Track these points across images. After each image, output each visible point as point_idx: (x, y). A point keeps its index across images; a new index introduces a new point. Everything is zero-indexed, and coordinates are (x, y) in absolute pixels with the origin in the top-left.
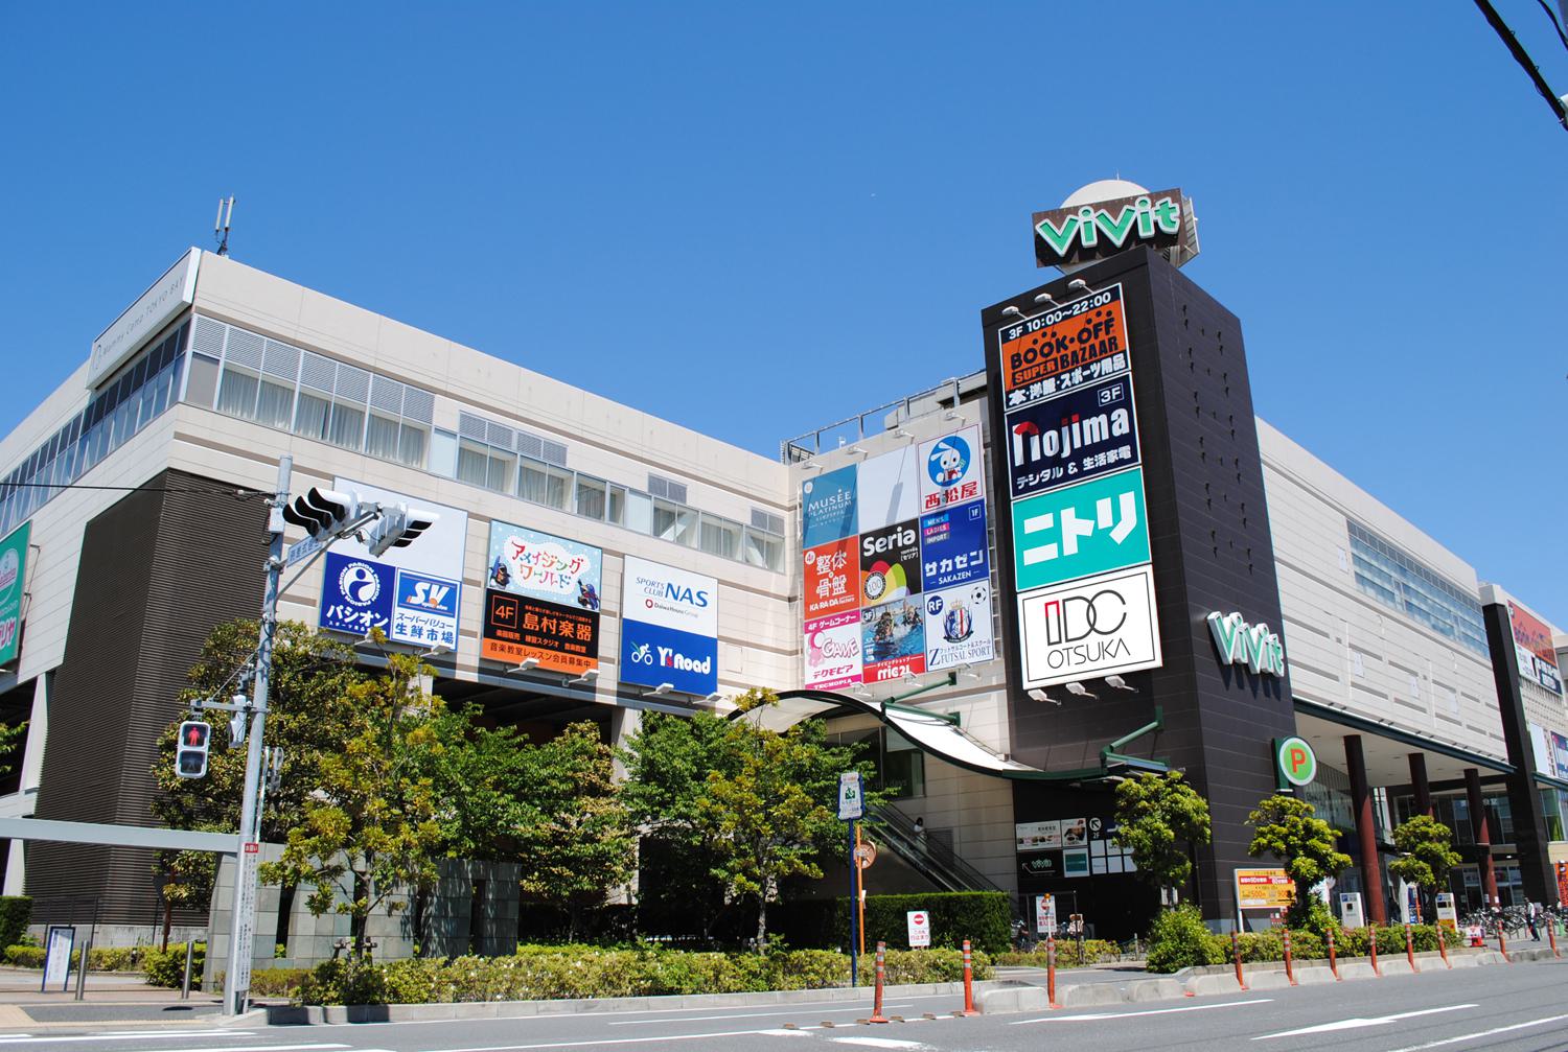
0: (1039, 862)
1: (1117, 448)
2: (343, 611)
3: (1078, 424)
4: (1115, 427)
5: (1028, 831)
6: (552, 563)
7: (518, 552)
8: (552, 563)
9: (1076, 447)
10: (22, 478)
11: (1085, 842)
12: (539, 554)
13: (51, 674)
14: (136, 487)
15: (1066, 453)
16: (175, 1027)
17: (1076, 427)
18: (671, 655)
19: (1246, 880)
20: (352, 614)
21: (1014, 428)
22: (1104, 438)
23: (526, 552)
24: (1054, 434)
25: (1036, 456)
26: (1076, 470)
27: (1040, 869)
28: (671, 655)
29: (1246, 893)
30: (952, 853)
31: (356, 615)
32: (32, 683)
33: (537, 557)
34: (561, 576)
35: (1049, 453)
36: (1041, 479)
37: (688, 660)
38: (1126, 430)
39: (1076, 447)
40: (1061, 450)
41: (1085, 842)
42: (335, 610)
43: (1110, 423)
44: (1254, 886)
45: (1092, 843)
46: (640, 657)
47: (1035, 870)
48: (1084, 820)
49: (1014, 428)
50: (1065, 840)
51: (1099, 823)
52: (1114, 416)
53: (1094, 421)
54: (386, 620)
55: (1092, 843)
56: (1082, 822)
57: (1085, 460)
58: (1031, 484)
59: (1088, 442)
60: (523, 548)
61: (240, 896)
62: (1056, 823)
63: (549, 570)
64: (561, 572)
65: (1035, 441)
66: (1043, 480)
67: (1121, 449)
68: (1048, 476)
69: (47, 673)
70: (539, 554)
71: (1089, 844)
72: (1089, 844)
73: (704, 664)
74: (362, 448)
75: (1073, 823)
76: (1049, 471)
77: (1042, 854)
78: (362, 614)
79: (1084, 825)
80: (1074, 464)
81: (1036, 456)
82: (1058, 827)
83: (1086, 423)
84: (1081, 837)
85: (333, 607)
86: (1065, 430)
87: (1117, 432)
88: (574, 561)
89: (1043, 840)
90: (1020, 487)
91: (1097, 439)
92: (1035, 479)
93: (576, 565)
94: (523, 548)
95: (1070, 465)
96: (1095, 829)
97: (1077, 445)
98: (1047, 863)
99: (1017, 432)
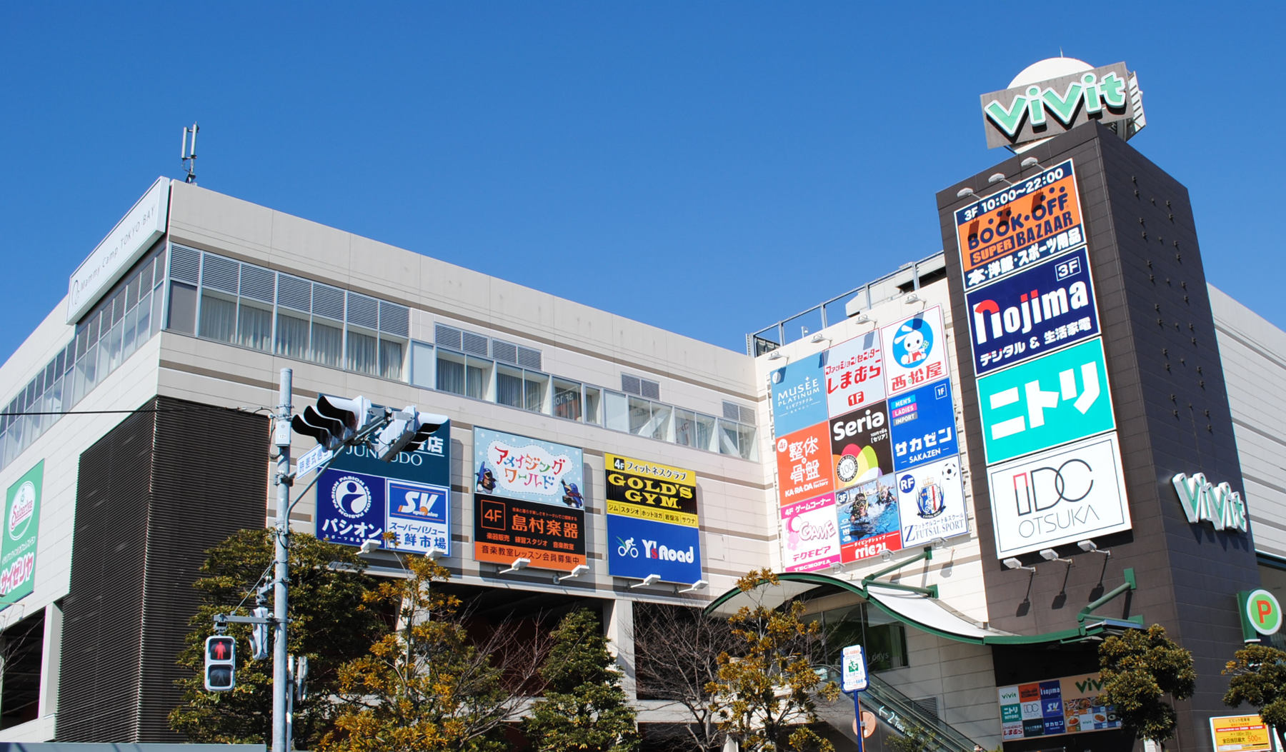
1: (1077, 320)
2: (337, 524)
4: (1074, 299)
6: (535, 465)
7: (502, 457)
8: (535, 465)
12: (522, 458)
13: (59, 603)
15: (1027, 328)
17: (1035, 302)
18: (655, 547)
22: (1055, 315)
23: (509, 456)
24: (1013, 310)
25: (997, 333)
28: (655, 547)
33: (520, 460)
34: (545, 477)
36: (1004, 355)
37: (672, 551)
38: (1085, 302)
40: (1022, 326)
43: (1069, 297)
46: (626, 551)
49: (975, 307)
52: (1072, 289)
53: (1053, 295)
59: (1048, 316)
60: (506, 452)
63: (532, 472)
64: (545, 474)
65: (995, 318)
66: (1006, 356)
67: (1081, 321)
70: (522, 458)
73: (688, 553)
74: (690, 446)
76: (1011, 346)
78: (356, 526)
80: (1035, 338)
81: (997, 333)
83: (1045, 298)
85: (327, 521)
86: (1025, 306)
87: (1076, 305)
88: (556, 463)
93: (558, 466)
94: (506, 452)
98: (1006, 718)
99: (978, 310)
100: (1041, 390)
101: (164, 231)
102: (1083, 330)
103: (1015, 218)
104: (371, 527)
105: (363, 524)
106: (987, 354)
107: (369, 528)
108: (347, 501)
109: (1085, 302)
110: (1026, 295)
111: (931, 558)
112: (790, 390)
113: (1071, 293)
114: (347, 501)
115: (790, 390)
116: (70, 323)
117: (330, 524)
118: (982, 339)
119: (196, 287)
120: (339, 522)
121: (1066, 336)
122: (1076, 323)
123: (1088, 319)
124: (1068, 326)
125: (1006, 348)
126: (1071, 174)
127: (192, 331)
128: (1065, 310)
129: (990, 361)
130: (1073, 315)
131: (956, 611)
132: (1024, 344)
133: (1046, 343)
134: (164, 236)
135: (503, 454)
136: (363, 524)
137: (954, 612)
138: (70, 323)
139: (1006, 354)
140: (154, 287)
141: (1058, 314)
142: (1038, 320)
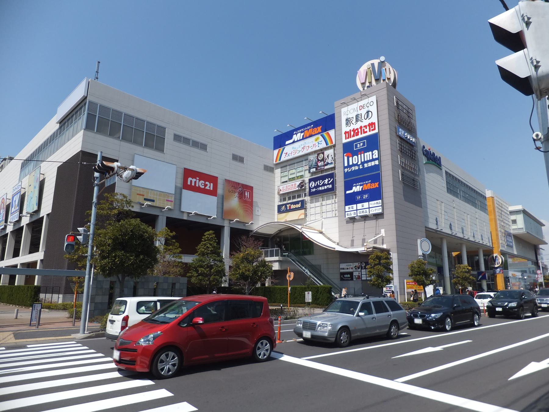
0: (346, 275)
1: (374, 161)
2: (319, 182)
3: (360, 155)
4: (374, 155)
5: (343, 266)
9: (345, 166)
10: (31, 159)
11: (360, 270)
13: (48, 215)
14: (64, 162)
15: (359, 163)
16: (52, 340)
17: (362, 155)
19: (409, 283)
20: (322, 182)
21: (345, 154)
22: (370, 159)
23: (288, 154)
24: (356, 157)
25: (351, 163)
26: (362, 167)
27: (347, 278)
29: (408, 287)
30: (321, 272)
31: (323, 181)
32: (43, 217)
35: (355, 163)
36: (352, 169)
37: (295, 205)
38: (377, 157)
39: (345, 166)
40: (358, 162)
41: (360, 270)
42: (317, 183)
43: (373, 154)
44: (411, 285)
45: (362, 270)
47: (345, 278)
48: (360, 263)
49: (345, 154)
50: (354, 269)
51: (364, 264)
52: (374, 152)
53: (368, 153)
54: (332, 179)
55: (362, 270)
56: (359, 264)
57: (365, 164)
58: (349, 171)
59: (366, 160)
60: (287, 153)
61: (356, 138)
62: (352, 264)
65: (350, 158)
66: (352, 170)
67: (376, 161)
68: (354, 169)
69: (47, 215)
71: (361, 270)
72: (361, 270)
73: (299, 204)
74: (372, 215)
75: (357, 264)
76: (354, 167)
77: (347, 273)
78: (325, 181)
79: (360, 265)
80: (361, 165)
81: (351, 163)
82: (352, 265)
83: (366, 154)
84: (359, 268)
85: (316, 182)
86: (359, 156)
87: (374, 157)
89: (348, 269)
90: (345, 172)
91: (368, 159)
92: (350, 169)
95: (360, 166)
96: (363, 266)
97: (363, 161)
98: (349, 276)
99: (346, 156)
100: (253, 187)
101: (86, 96)
102: (376, 164)
103: (355, 129)
104: (329, 179)
105: (327, 179)
106: (347, 169)
107: (329, 180)
108: (312, 185)
109: (377, 157)
110: (360, 152)
111: (351, 240)
112: (371, 126)
113: (373, 153)
114: (312, 185)
115: (371, 126)
116: (57, 123)
117: (317, 183)
118: (346, 165)
119: (96, 116)
120: (320, 181)
121: (371, 166)
122: (374, 162)
123: (378, 161)
124: (372, 162)
125: (352, 167)
126: (16, 339)
127: (143, 145)
128: (371, 158)
129: (347, 171)
130: (373, 160)
131: (329, 238)
132: (358, 167)
133: (365, 167)
134: (86, 97)
135: (286, 154)
136: (327, 179)
137: (329, 239)
138: (57, 123)
139: (352, 169)
140: (82, 114)
141: (369, 159)
142: (363, 161)
